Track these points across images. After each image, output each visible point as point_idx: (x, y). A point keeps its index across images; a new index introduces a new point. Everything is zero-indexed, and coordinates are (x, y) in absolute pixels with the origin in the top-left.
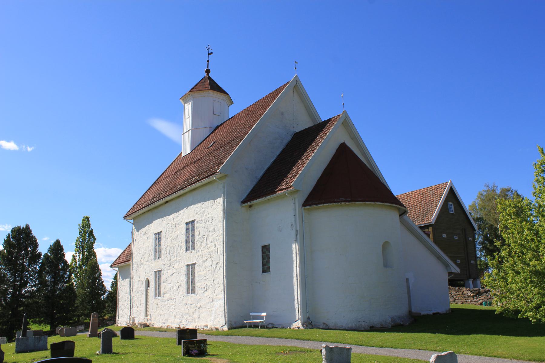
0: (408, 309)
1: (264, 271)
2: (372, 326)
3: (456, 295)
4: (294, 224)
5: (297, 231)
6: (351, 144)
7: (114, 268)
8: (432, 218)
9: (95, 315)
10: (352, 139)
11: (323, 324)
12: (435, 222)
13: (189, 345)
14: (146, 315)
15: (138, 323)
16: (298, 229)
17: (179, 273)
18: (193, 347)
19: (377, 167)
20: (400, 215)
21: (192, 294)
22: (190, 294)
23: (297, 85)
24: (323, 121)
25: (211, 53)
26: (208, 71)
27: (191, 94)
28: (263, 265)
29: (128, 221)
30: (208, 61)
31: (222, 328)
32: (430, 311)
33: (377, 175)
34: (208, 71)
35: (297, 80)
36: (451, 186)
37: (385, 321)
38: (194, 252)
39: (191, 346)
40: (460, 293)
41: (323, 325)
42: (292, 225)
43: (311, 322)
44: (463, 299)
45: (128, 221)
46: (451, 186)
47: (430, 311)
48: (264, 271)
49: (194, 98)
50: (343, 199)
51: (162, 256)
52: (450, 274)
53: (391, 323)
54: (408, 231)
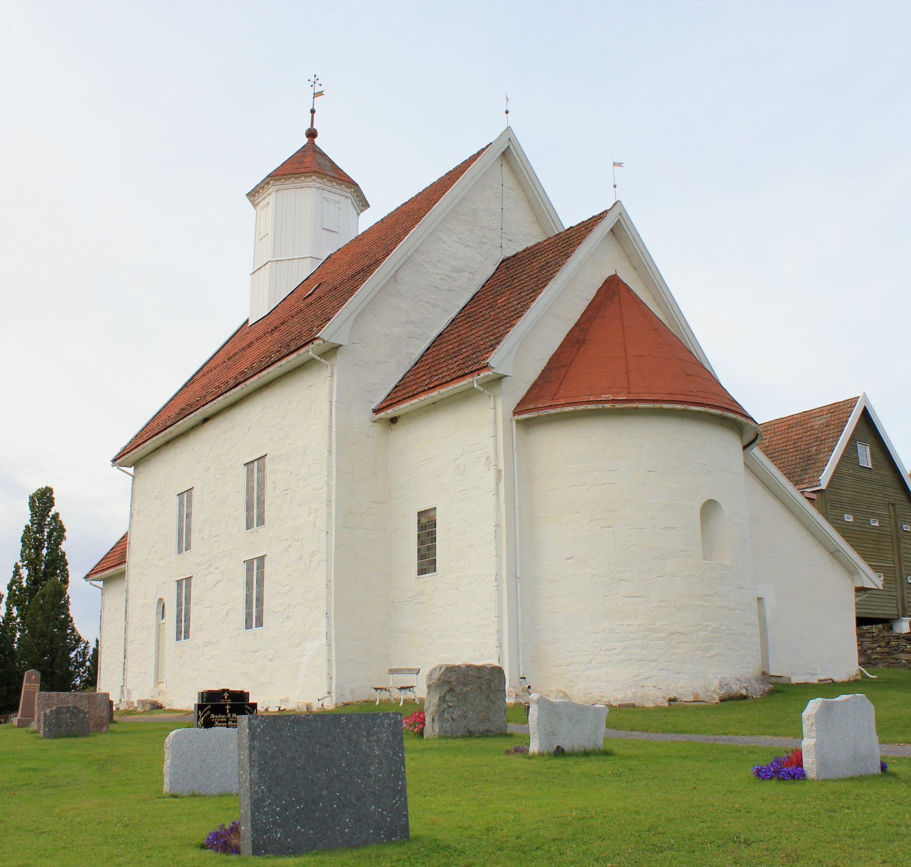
0: (760, 661)
1: (422, 571)
2: (672, 697)
3: (873, 649)
4: (492, 457)
5: (499, 471)
6: (628, 278)
7: (93, 582)
8: (820, 476)
9: (33, 677)
10: (635, 269)
11: (557, 691)
12: (828, 487)
13: (213, 716)
14: (158, 682)
15: (139, 701)
16: (502, 466)
17: (228, 582)
18: (222, 720)
19: (693, 335)
20: (745, 447)
21: (257, 628)
22: (252, 628)
23: (511, 150)
24: (567, 227)
25: (321, 93)
26: (312, 134)
27: (271, 182)
28: (421, 556)
29: (122, 470)
30: (313, 111)
31: (321, 702)
32: (811, 674)
33: (689, 346)
34: (312, 134)
35: (508, 135)
36: (865, 407)
37: (705, 688)
38: (261, 529)
39: (217, 717)
40: (883, 644)
41: (557, 693)
42: (488, 458)
43: (529, 687)
44: (888, 657)
45: (122, 470)
46: (865, 407)
47: (811, 674)
48: (422, 571)
49: (278, 190)
50: (609, 397)
51: (193, 544)
52: (859, 590)
53: (718, 690)
54: (763, 487)
